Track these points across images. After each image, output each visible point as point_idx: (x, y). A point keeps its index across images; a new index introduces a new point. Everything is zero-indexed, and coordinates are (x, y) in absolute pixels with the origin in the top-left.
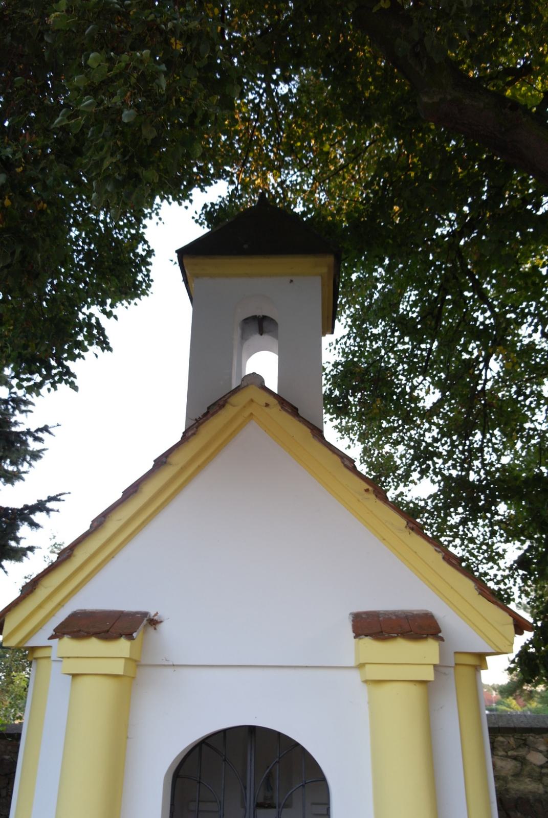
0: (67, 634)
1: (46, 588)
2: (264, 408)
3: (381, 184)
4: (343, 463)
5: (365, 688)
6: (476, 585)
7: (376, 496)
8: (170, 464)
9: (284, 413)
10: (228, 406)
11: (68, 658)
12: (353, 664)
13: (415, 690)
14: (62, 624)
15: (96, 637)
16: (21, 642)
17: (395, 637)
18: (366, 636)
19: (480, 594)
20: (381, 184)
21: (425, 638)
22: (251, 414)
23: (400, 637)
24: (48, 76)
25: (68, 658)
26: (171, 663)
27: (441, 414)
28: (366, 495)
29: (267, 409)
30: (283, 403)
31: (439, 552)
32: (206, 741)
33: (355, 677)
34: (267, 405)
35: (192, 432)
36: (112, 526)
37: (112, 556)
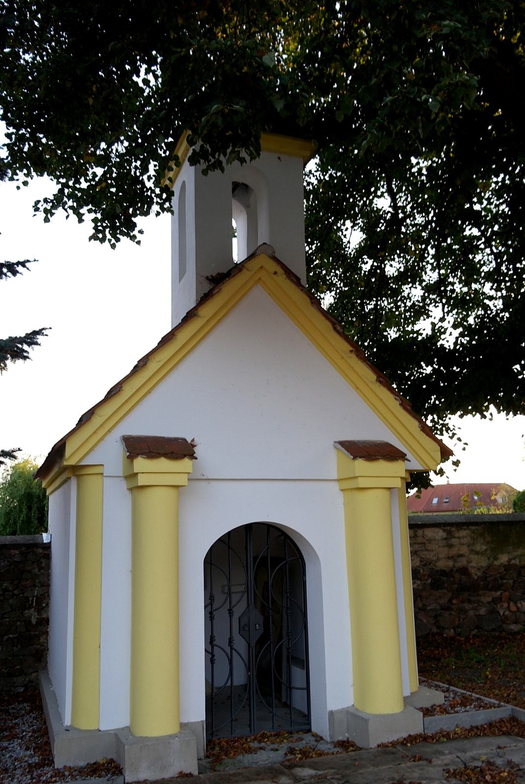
0: (142, 454)
1: (100, 416)
2: (273, 275)
3: (349, 82)
4: (335, 328)
5: (341, 493)
6: (420, 424)
7: (357, 356)
8: (199, 317)
9: (288, 281)
10: (244, 271)
11: (143, 473)
12: (359, 478)
13: (386, 493)
14: (346, 450)
15: (165, 457)
16: (80, 460)
17: (379, 459)
18: (360, 458)
19: (421, 430)
20: (349, 82)
21: (397, 460)
22: (260, 279)
23: (381, 458)
24: (354, 126)
25: (143, 473)
26: (206, 478)
27: (50, 143)
28: (350, 355)
29: (275, 277)
30: (289, 274)
31: (398, 400)
32: (271, 528)
33: (335, 487)
34: (275, 273)
35: (217, 290)
36: (153, 366)
37: (149, 392)
